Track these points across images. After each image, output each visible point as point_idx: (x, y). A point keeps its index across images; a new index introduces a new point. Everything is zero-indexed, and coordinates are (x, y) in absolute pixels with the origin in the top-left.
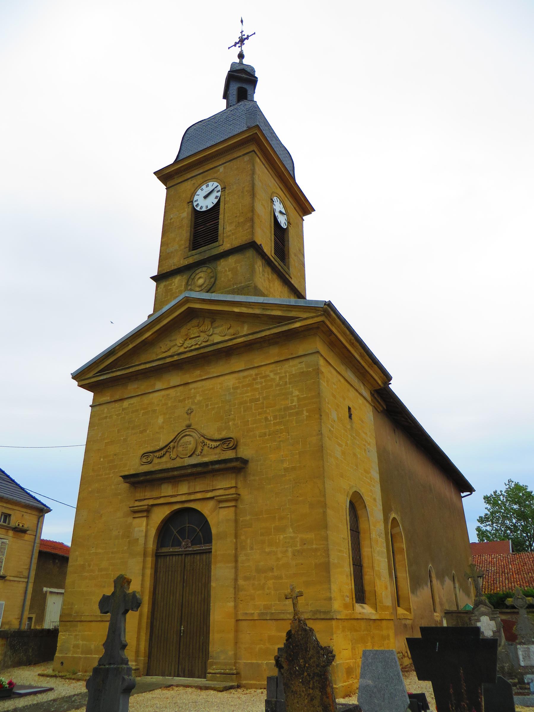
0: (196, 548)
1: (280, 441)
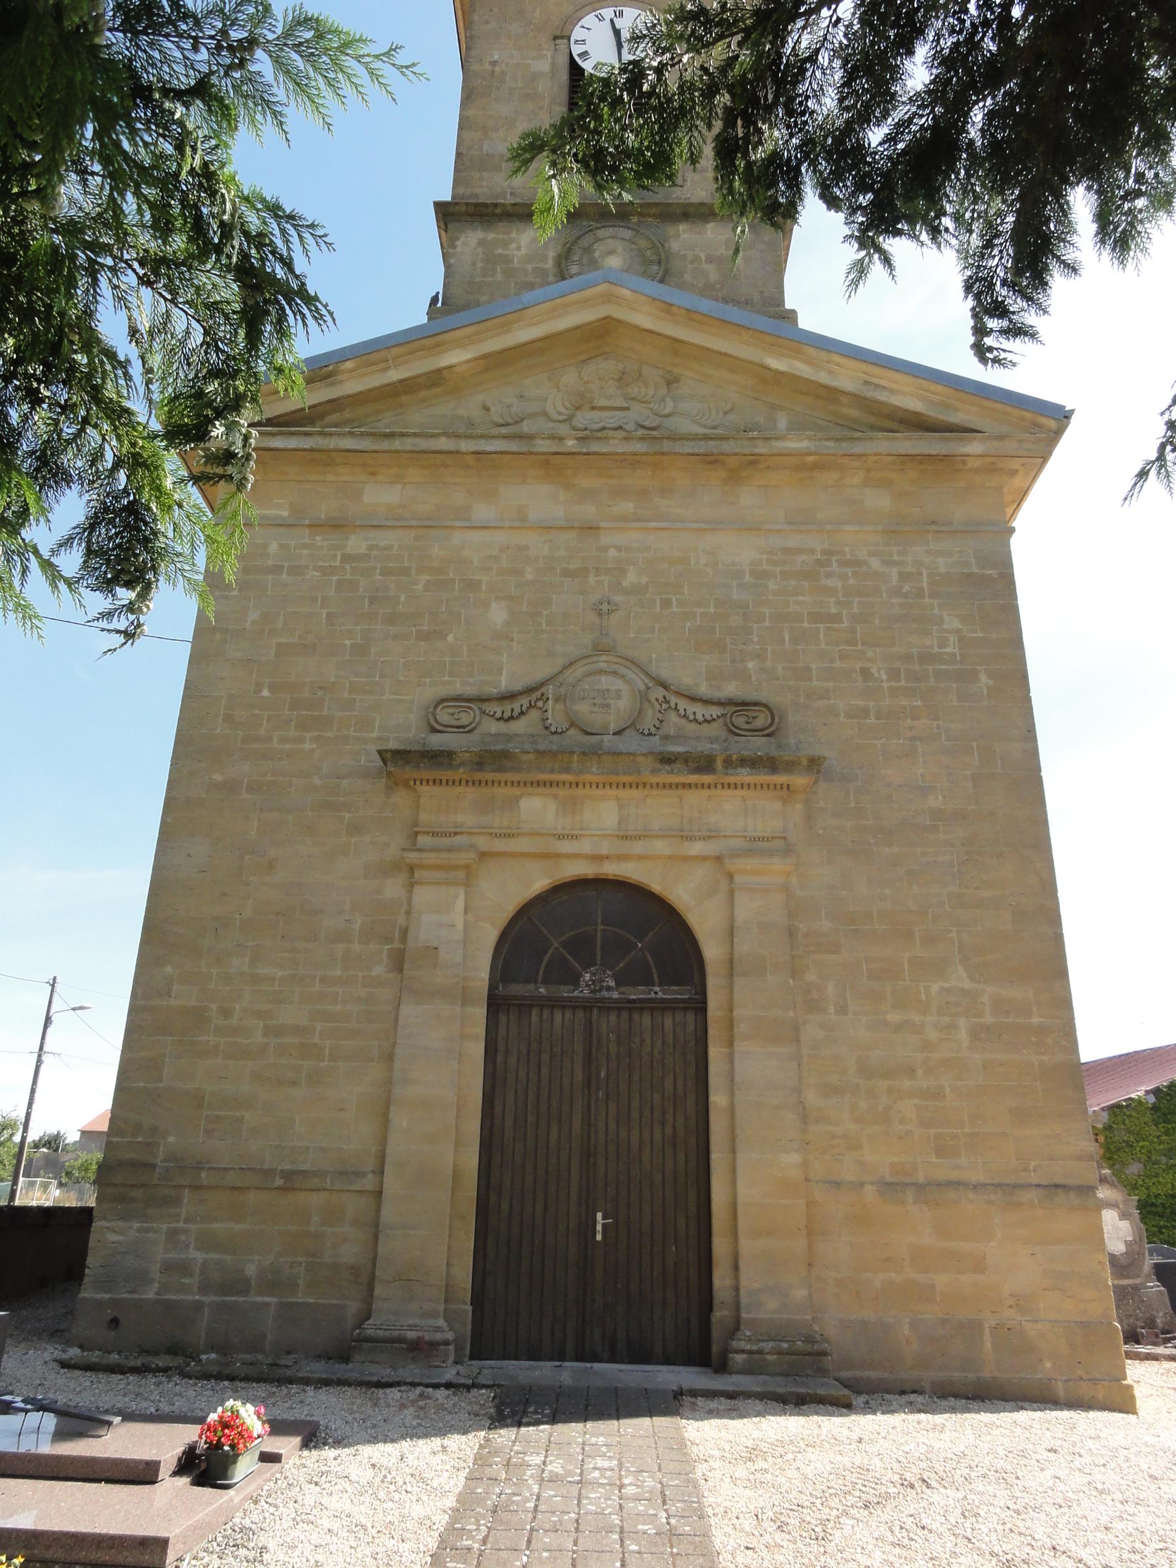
0: (635, 993)
1: (913, 739)
